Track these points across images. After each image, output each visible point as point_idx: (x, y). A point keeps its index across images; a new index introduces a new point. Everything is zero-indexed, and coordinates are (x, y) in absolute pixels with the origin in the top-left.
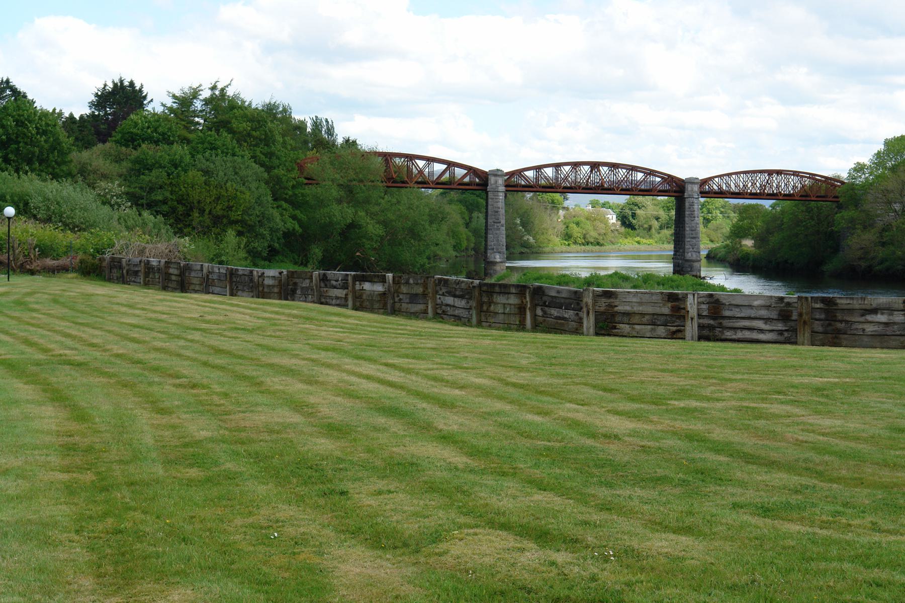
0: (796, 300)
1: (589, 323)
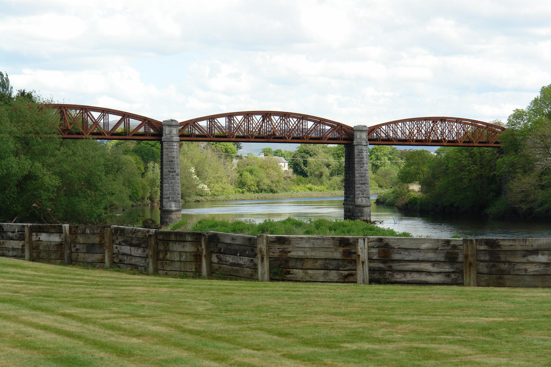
0: (461, 243)
1: (263, 268)
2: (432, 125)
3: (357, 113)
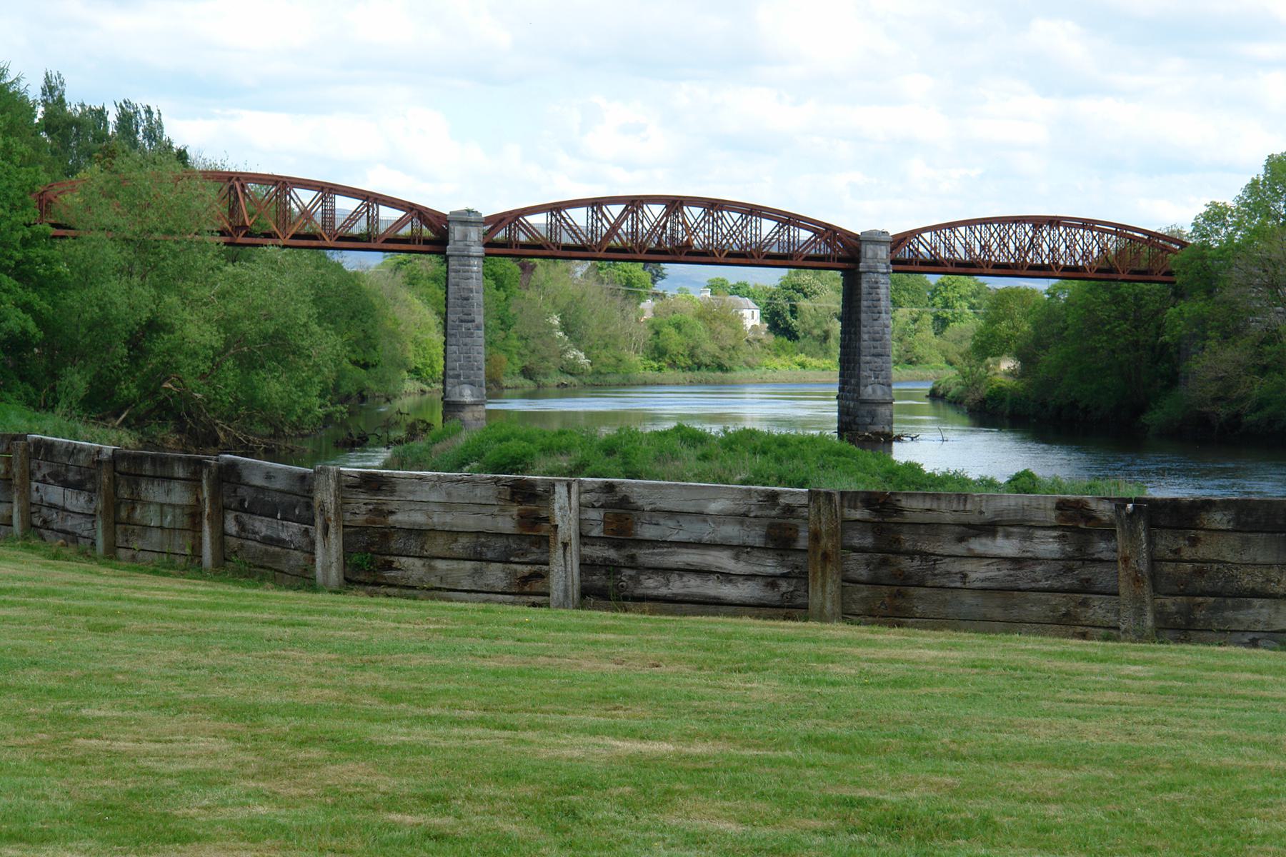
0: (805, 501)
1: (329, 557)
2: (1030, 234)
3: (868, 207)
